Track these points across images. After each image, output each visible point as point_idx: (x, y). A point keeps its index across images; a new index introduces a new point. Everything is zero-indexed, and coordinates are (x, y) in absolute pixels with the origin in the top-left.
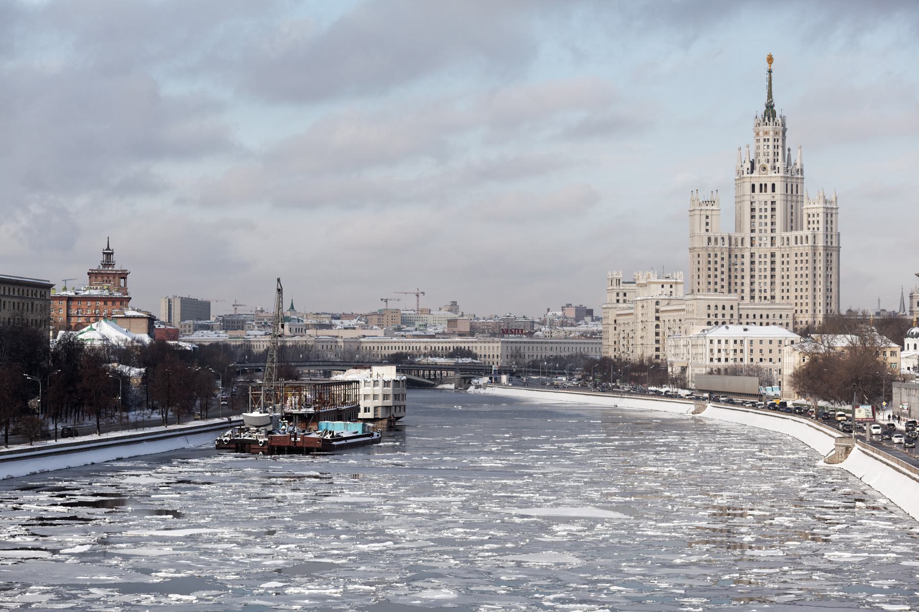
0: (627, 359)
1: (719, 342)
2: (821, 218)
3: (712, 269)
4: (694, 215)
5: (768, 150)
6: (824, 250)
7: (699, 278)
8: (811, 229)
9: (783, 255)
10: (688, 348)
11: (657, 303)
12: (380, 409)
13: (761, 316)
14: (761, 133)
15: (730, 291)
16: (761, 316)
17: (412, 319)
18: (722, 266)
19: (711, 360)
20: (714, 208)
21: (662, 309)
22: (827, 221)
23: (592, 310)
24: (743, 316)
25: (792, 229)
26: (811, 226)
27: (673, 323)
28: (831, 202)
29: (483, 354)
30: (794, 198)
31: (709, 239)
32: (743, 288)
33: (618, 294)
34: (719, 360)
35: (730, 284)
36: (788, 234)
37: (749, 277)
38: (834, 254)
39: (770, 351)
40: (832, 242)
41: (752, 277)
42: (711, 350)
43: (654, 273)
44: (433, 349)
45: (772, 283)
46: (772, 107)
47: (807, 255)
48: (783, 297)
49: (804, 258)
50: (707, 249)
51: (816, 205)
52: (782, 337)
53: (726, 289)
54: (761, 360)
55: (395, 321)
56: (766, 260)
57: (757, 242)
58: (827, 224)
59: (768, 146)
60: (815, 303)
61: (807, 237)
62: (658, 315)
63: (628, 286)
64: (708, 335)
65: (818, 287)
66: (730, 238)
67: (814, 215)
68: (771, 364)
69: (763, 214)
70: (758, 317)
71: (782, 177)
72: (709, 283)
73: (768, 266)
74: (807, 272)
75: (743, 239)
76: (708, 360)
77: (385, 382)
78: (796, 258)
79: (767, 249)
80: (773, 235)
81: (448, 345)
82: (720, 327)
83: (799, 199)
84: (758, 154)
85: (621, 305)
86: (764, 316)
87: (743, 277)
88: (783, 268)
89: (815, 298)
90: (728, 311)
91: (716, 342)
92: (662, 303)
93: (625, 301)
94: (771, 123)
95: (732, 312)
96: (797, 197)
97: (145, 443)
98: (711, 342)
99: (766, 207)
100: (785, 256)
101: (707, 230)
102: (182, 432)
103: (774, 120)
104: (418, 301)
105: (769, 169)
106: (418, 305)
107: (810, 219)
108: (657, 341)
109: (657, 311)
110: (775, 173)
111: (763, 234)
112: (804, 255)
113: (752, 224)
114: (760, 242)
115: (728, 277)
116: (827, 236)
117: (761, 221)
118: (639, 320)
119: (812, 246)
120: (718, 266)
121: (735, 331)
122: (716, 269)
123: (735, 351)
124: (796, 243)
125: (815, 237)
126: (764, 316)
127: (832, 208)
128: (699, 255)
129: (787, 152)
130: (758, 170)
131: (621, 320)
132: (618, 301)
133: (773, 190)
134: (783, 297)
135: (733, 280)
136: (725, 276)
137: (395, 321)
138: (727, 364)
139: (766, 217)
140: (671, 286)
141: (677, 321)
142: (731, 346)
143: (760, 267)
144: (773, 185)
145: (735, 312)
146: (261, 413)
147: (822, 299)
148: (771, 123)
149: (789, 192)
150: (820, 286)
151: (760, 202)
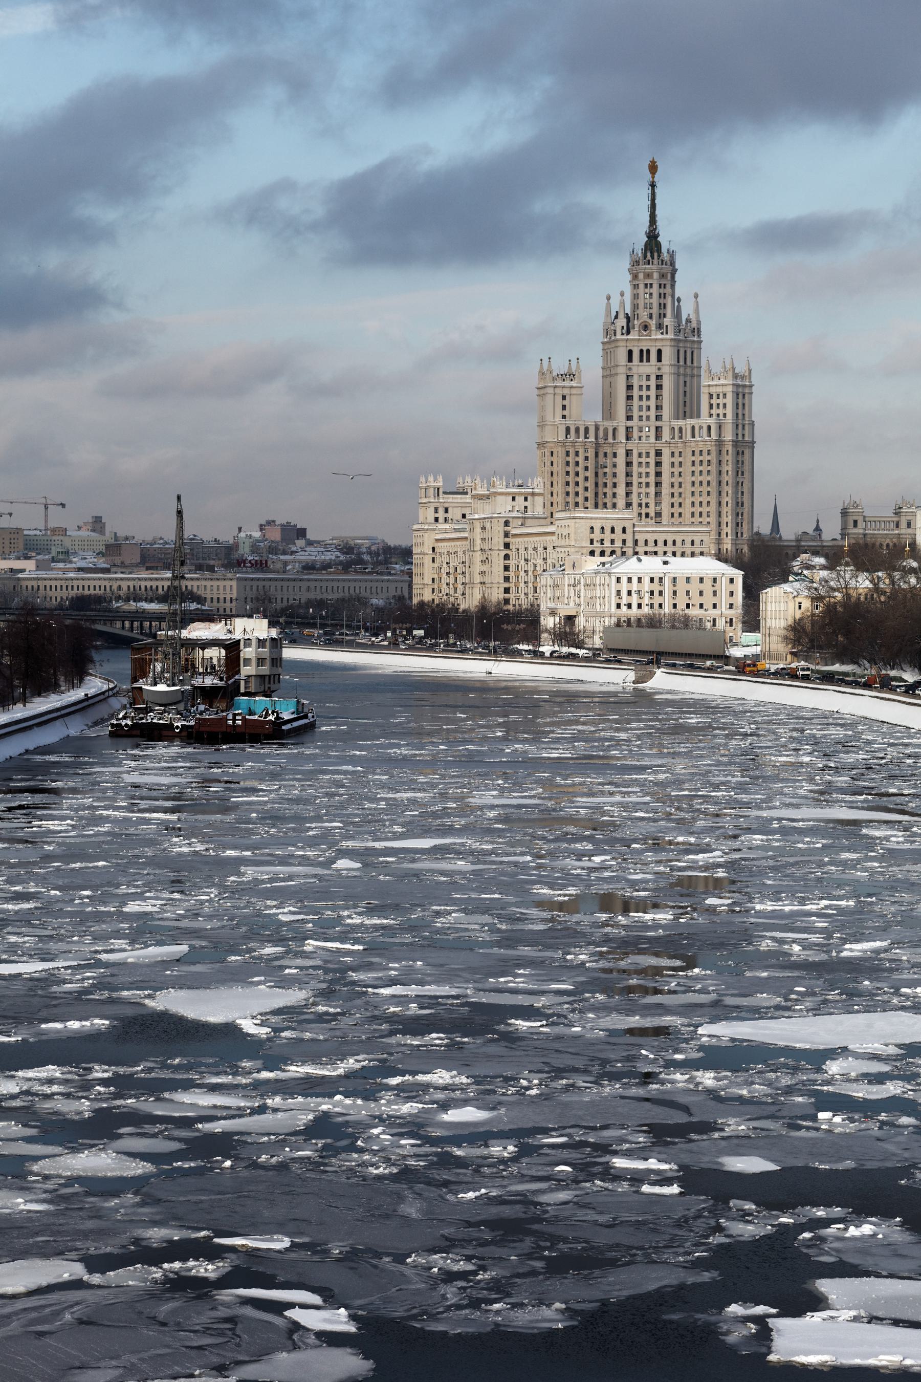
0: (453, 605)
1: (630, 580)
2: (729, 400)
3: (572, 474)
4: (545, 394)
5: (651, 301)
6: (733, 446)
7: (552, 486)
8: (715, 417)
9: (673, 453)
10: (577, 589)
11: (507, 523)
12: (252, 679)
13: (665, 543)
14: (641, 276)
15: (596, 506)
16: (665, 543)
17: (39, 543)
18: (586, 469)
19: (618, 606)
20: (574, 384)
21: (514, 532)
22: (737, 404)
23: (305, 530)
24: (639, 543)
25: (685, 416)
26: (714, 412)
27: (533, 552)
28: (743, 377)
29: (215, 597)
30: (689, 371)
31: (568, 430)
32: (614, 500)
33: (436, 510)
34: (629, 606)
35: (596, 494)
36: (681, 423)
37: (624, 485)
38: (747, 452)
39: (701, 593)
40: (743, 435)
41: (629, 484)
42: (618, 592)
43: (501, 479)
44: (132, 589)
45: (656, 493)
46: (657, 236)
47: (709, 454)
48: (672, 514)
49: (705, 458)
50: (564, 444)
51: (722, 382)
52: (718, 573)
53: (590, 504)
54: (688, 606)
55: (16, 545)
56: (648, 460)
57: (636, 434)
58: (737, 408)
59: (651, 294)
60: (720, 523)
61: (709, 428)
62: (507, 540)
63: (450, 499)
64: (613, 571)
65: (725, 499)
66: (597, 428)
67: (718, 395)
68: (702, 611)
69: (644, 393)
70: (660, 543)
71: (671, 339)
72: (568, 494)
73: (652, 470)
74: (709, 478)
75: (615, 430)
76: (614, 606)
77: (259, 640)
78: (693, 458)
79: (649, 444)
80: (659, 424)
81: (154, 584)
82: (628, 559)
83: (695, 372)
84: (635, 307)
85: (442, 526)
86: (670, 543)
87: (615, 485)
88: (673, 473)
89: (720, 516)
90: (618, 536)
91: (624, 580)
92: (513, 523)
93: (446, 520)
94: (655, 261)
95: (624, 536)
96: (693, 368)
97: (35, 728)
98: (618, 580)
99: (648, 383)
100: (677, 454)
101: (564, 417)
102: (59, 714)
103: (659, 256)
104: (46, 516)
105: (653, 328)
106: (46, 521)
107: (712, 401)
108: (507, 579)
109: (507, 535)
110: (662, 333)
111: (644, 423)
112: (705, 453)
113: (629, 408)
114: (641, 434)
115: (593, 486)
116: (737, 426)
117: (641, 403)
118: (477, 548)
119: (716, 441)
120: (580, 469)
121: (651, 565)
122: (577, 474)
123: (652, 593)
124: (693, 436)
125: (720, 427)
126: (670, 543)
127: (744, 386)
128: (552, 453)
129: (676, 304)
130: (636, 329)
131: (442, 547)
132: (436, 520)
133: (659, 359)
134: (672, 514)
135: (601, 490)
136: (590, 484)
137: (16, 545)
138: (640, 611)
139: (648, 398)
140: (526, 499)
141: (540, 550)
142: (647, 586)
143: (640, 470)
144: (659, 352)
145: (629, 537)
146: (168, 685)
147: (730, 517)
148: (655, 261)
149: (682, 362)
150: (728, 499)
151: (640, 376)
